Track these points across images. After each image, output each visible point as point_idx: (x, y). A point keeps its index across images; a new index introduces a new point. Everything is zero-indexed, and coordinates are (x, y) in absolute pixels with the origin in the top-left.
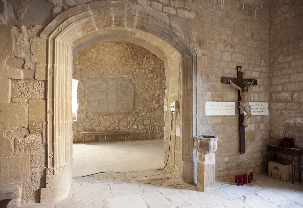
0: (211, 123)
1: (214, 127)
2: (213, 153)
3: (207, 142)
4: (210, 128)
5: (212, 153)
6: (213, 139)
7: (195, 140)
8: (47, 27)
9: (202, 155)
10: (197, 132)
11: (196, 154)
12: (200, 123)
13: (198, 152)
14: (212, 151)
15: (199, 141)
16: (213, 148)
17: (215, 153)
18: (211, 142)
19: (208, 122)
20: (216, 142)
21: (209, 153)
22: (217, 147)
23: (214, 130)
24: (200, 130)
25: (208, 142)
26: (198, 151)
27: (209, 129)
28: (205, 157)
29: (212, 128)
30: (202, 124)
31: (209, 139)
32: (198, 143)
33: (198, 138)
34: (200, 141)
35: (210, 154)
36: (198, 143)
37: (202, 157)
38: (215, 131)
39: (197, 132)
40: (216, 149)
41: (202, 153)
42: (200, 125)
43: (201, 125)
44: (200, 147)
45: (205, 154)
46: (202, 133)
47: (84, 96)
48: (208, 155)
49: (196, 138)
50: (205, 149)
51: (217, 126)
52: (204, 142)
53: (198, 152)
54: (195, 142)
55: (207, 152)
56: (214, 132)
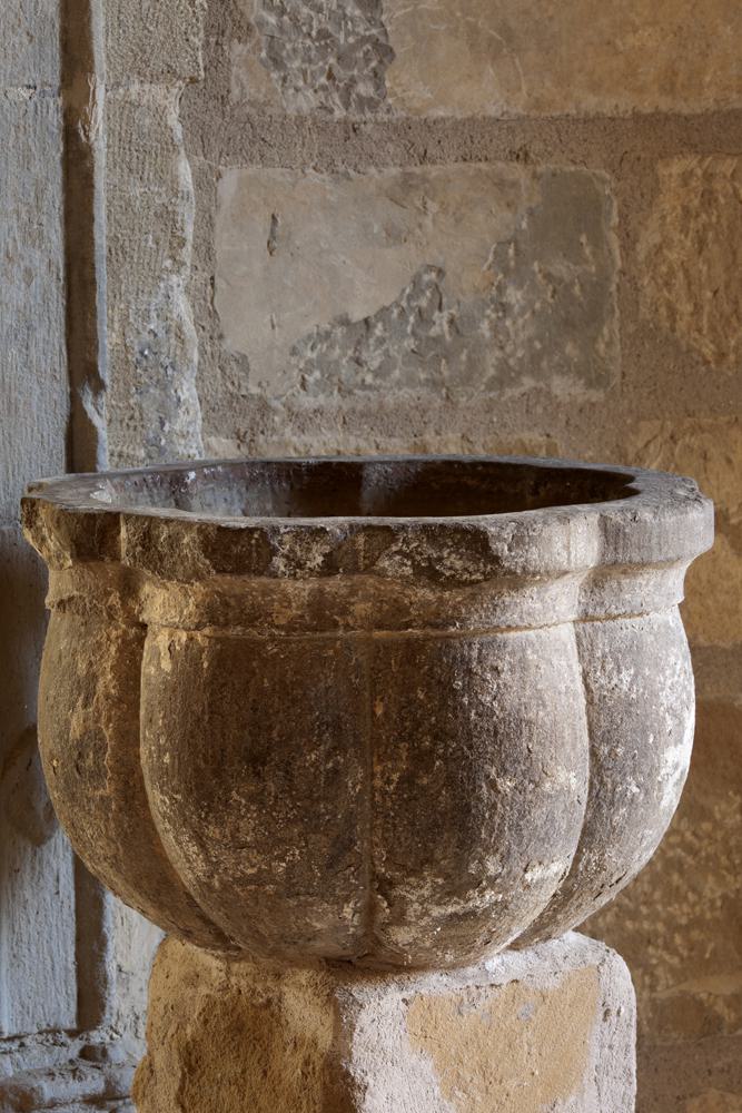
0: (484, 95)
1: (569, 215)
2: (570, 940)
3: (395, 615)
4: (465, 239)
5: (541, 930)
6: (573, 538)
7: (61, 581)
8: (141, 700)
9: (270, 1010)
10: (82, 369)
11: (90, 1003)
12: (168, 102)
13: (134, 937)
14: (551, 871)
15: (168, 613)
16: (570, 778)
17: (620, 930)
18: (529, 602)
19: (413, 89)
20: (659, 608)
21: (464, 936)
22: (677, 757)
23: (575, 316)
24: (182, 307)
25: (438, 620)
26: (159, 891)
27: (430, 286)
28: (362, 1062)
29: (511, 261)
30: (226, 127)
31: (478, 544)
32: (158, 663)
33: (147, 531)
34: (213, 614)
35: (500, 963)
36: (158, 663)
37: (290, 1067)
38: (611, 329)
39: (82, 369)
40: (670, 797)
41: (283, 952)
42: (185, 171)
43: (206, 181)
44: (205, 788)
45: (368, 960)
46: (235, 407)
47: (275, 640)
48: (433, 984)
49: (93, 537)
50: (344, 845)
51: (669, 203)
52: (322, 613)
53: (134, 937)
54: (63, 655)
55: (421, 912)
56: (596, 379)
